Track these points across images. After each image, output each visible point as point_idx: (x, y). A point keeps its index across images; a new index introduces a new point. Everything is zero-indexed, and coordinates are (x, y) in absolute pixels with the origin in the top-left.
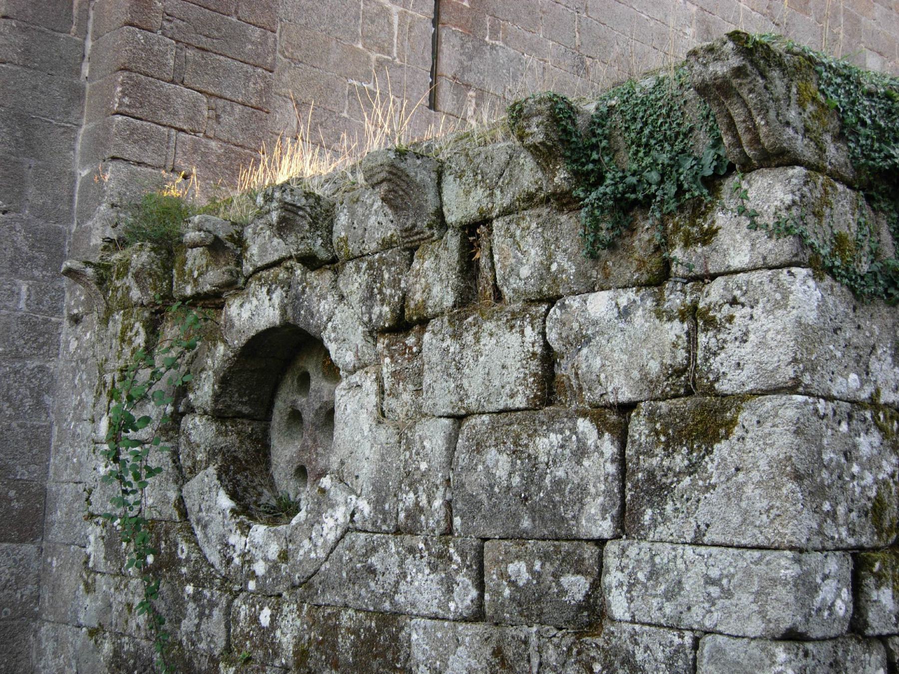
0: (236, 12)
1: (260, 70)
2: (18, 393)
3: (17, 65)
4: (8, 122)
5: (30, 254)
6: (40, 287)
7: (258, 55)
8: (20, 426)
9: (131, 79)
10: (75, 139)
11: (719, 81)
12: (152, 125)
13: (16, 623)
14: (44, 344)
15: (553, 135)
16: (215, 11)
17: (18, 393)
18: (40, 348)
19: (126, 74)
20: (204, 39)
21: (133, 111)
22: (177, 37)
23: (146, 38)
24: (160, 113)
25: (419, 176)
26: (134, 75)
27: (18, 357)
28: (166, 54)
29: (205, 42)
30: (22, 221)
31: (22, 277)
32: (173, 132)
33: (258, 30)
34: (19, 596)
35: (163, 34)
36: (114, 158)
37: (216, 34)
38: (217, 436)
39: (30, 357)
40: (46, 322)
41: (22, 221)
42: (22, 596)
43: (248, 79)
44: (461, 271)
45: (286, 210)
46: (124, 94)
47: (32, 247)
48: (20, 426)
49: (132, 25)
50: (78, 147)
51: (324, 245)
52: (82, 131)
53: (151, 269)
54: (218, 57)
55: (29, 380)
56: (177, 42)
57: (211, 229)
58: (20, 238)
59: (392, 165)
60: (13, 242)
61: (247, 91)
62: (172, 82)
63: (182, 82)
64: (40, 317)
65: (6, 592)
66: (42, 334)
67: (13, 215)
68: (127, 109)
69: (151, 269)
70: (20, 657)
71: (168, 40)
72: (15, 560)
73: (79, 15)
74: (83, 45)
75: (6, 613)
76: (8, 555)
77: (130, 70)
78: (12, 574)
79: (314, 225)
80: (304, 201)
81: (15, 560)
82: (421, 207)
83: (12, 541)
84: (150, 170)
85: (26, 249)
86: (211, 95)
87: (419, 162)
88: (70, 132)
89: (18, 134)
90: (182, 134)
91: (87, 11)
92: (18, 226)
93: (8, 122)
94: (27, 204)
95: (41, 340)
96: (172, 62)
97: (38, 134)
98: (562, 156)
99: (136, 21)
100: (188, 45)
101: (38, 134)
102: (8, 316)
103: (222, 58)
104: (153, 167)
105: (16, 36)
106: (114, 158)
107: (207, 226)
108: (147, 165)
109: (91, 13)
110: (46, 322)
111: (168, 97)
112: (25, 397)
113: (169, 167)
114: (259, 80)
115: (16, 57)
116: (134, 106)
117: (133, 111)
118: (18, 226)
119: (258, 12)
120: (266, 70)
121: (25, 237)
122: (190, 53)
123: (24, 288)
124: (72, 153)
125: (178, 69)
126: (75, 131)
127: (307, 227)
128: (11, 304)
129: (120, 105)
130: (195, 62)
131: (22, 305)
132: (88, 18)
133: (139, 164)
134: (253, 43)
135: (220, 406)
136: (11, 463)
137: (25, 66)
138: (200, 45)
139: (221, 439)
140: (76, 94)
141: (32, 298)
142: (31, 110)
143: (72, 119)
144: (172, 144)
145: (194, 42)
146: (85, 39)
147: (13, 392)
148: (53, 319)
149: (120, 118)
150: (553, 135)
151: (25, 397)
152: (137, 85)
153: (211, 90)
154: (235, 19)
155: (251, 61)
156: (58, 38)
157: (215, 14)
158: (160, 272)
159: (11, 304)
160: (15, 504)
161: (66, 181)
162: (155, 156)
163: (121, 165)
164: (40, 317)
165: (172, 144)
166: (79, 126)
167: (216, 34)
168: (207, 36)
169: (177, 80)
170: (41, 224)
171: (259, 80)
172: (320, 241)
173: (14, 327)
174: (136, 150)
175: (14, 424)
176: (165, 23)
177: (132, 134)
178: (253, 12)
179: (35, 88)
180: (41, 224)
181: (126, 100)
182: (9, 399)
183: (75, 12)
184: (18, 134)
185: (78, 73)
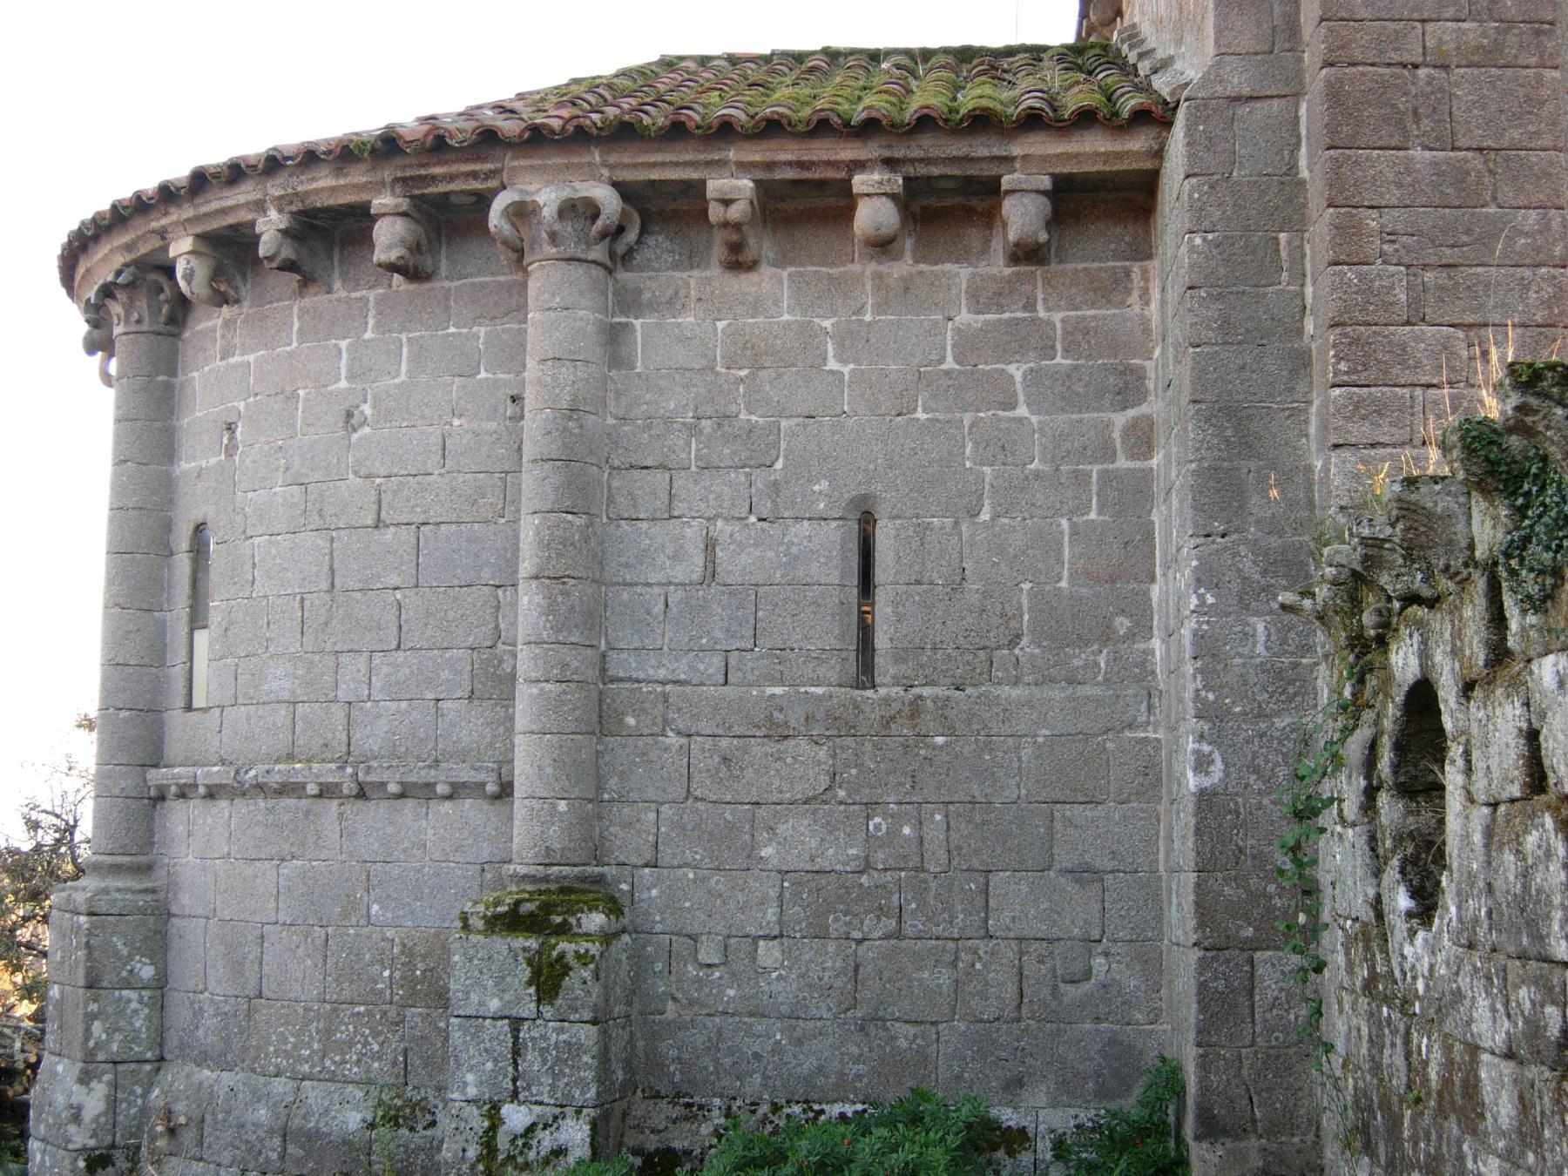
0: (1494, 198)
1: (1543, 270)
2: (1267, 761)
3: (1216, 344)
4: (1214, 421)
5: (1263, 582)
6: (1281, 622)
7: (1538, 250)
8: (1275, 803)
9: (1346, 335)
10: (1306, 422)
11: (1511, 422)
12: (1385, 389)
13: (1291, 1051)
14: (1295, 694)
15: (1474, 469)
16: (1460, 207)
17: (1267, 761)
18: (1290, 700)
19: (1338, 330)
20: (1448, 251)
21: (1354, 377)
22: (1406, 260)
23: (1360, 275)
24: (1394, 371)
25: (1440, 505)
26: (1349, 329)
27: (1262, 715)
28: (1392, 288)
29: (1449, 255)
30: (1246, 542)
31: (1256, 613)
32: (1418, 391)
33: (1533, 214)
34: (1292, 1017)
35: (1384, 262)
36: (1336, 446)
37: (1465, 238)
38: (1405, 817)
39: (1278, 713)
40: (1296, 665)
41: (1246, 542)
42: (1296, 1018)
43: (1526, 288)
44: (1490, 621)
45: (1367, 546)
46: (1339, 359)
47: (1265, 572)
48: (1275, 803)
49: (1336, 264)
50: (1312, 430)
51: (1425, 580)
52: (1314, 409)
53: (1335, 605)
54: (1473, 270)
55: (1280, 742)
56: (1408, 267)
57: (1344, 562)
58: (1247, 565)
59: (1399, 500)
60: (1239, 571)
61: (1527, 305)
62: (1408, 323)
63: (1423, 320)
64: (1286, 660)
65: (1275, 1012)
66: (1291, 682)
67: (1235, 536)
68: (1345, 378)
69: (1335, 605)
70: (1300, 1094)
71: (1392, 268)
72: (1283, 972)
73: (1289, 255)
74: (1302, 295)
75: (1277, 1039)
76: (1273, 965)
77: (1343, 324)
78: (1281, 990)
79: (1408, 557)
80: (1389, 530)
81: (1283, 972)
82: (1450, 542)
83: (1277, 948)
84: (1389, 450)
85: (1257, 577)
86: (1470, 326)
87: (1437, 488)
88: (1298, 414)
89: (1229, 433)
90: (1431, 391)
91: (1301, 247)
92: (1243, 550)
93: (1214, 421)
94: (1252, 519)
95: (1291, 690)
96: (1403, 297)
97: (1255, 427)
98: (1496, 489)
99: (1343, 257)
100: (1425, 267)
101: (1255, 427)
102: (1244, 665)
103: (1480, 270)
104: (1394, 446)
105: (1208, 308)
106: (1336, 446)
107: (1338, 559)
108: (1384, 445)
109: (1307, 248)
110: (1296, 665)
111: (1403, 347)
112: (1277, 764)
113: (1417, 441)
114: (1544, 285)
115: (1211, 334)
116: (1355, 371)
117: (1354, 377)
118: (1243, 550)
119: (1528, 187)
120: (1555, 266)
121: (1254, 562)
122: (1429, 276)
123: (1260, 628)
124: (1304, 440)
125: (1415, 303)
126: (1306, 411)
127: (1400, 561)
128: (1246, 650)
129: (1335, 375)
130: (1438, 287)
131: (1260, 649)
132: (1303, 256)
133: (1373, 446)
134: (1527, 235)
135: (1402, 779)
136: (1267, 850)
137: (1225, 343)
138: (1444, 261)
139: (1411, 819)
140: (1301, 362)
141: (1273, 638)
142: (1241, 397)
143: (1299, 396)
144: (1418, 408)
145: (1433, 260)
146: (1303, 285)
147: (1260, 761)
148: (1304, 661)
149: (1337, 391)
150: (1474, 469)
151: (1277, 764)
152: (1356, 341)
153: (1469, 319)
154: (1492, 210)
155: (1528, 261)
156: (1265, 295)
157: (1460, 212)
158: (1347, 607)
159: (1246, 650)
160: (1277, 901)
161: (1299, 479)
162: (1394, 430)
163: (1345, 453)
164: (1286, 660)
165: (1418, 408)
166: (1310, 402)
167: (1465, 238)
168: (1453, 246)
169: (1413, 320)
170: (1274, 542)
171: (1544, 285)
172: (1419, 576)
173: (1252, 679)
174: (1366, 428)
175: (1266, 801)
176: (1385, 247)
177: (1356, 408)
178: (1521, 189)
179: (1243, 368)
180: (1274, 542)
181: (1343, 366)
182: (1256, 770)
183: (1284, 254)
184: (1229, 433)
185: (1300, 332)
